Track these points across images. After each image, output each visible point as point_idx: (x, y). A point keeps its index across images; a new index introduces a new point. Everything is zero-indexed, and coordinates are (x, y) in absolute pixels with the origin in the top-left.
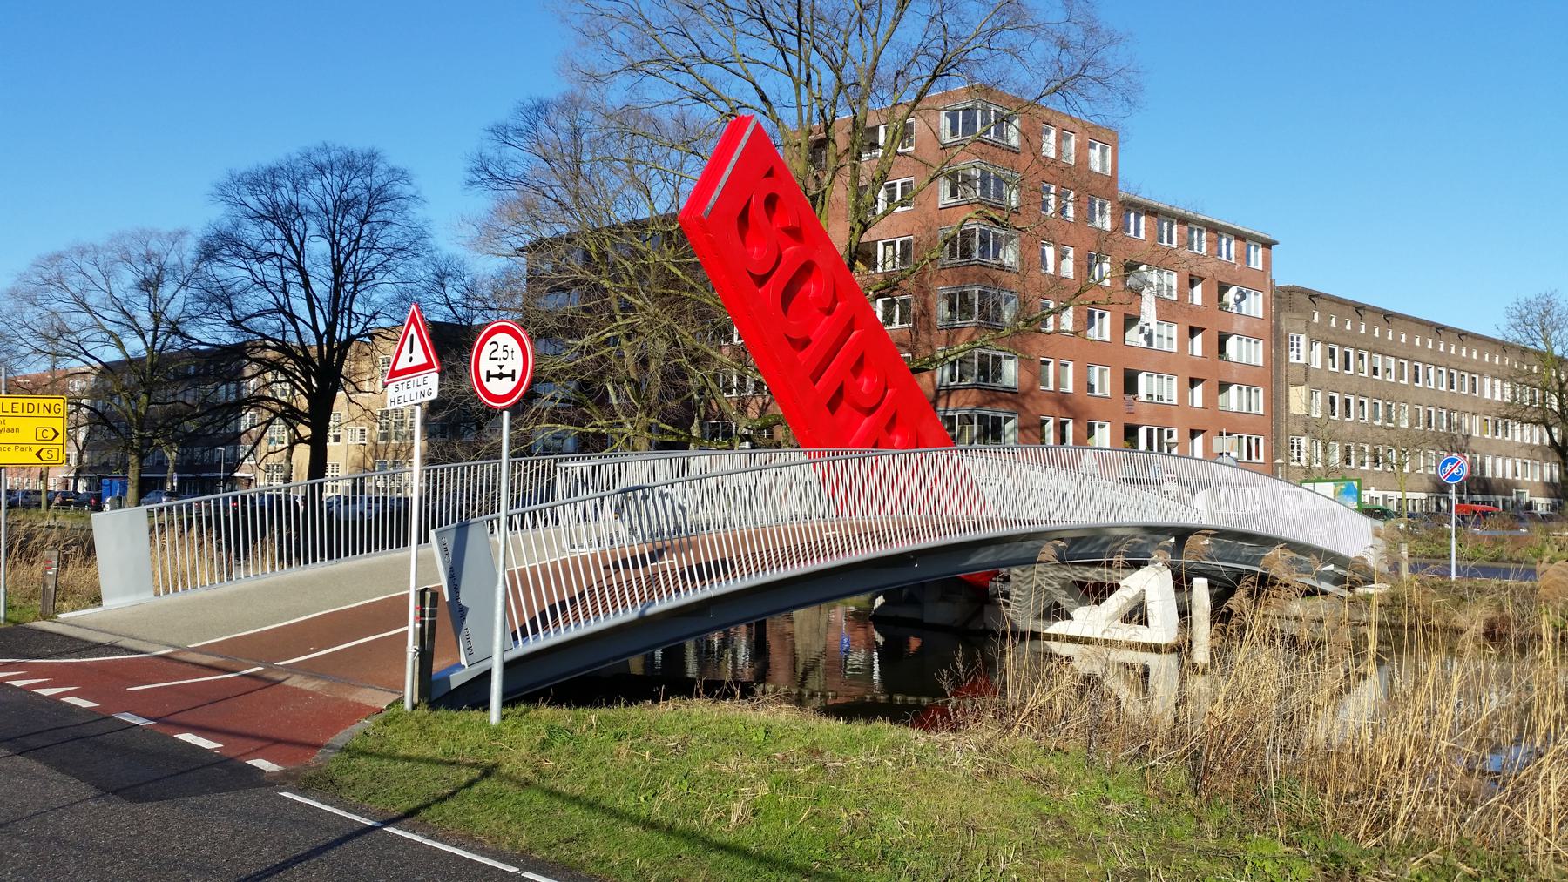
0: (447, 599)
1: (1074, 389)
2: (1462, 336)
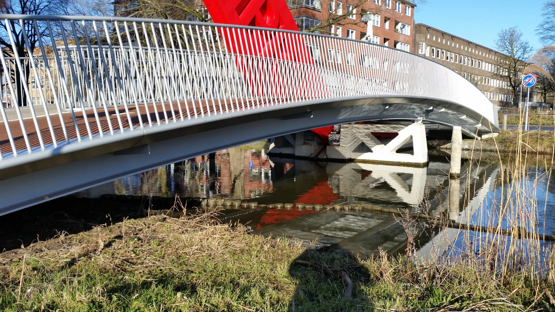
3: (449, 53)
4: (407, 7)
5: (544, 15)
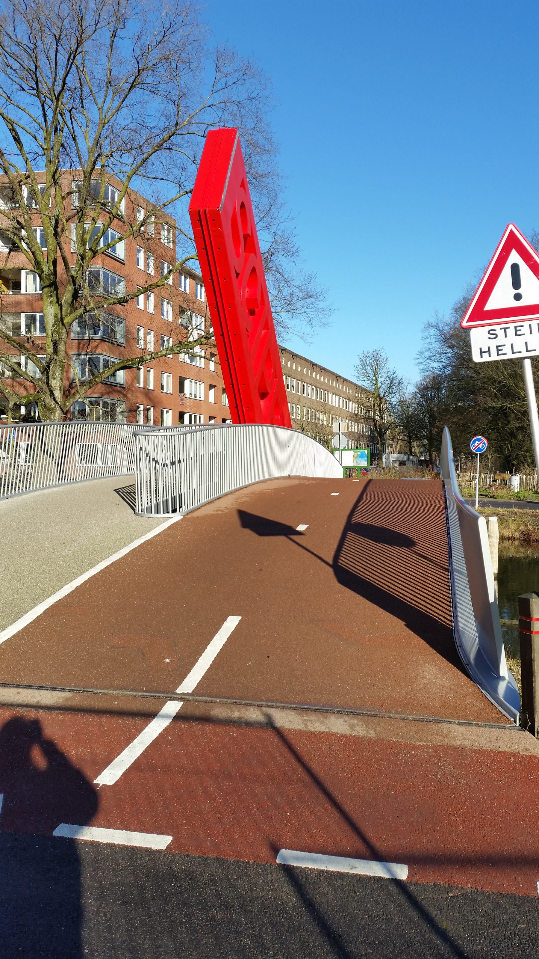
0: (338, 494)
1: (154, 387)
2: (323, 370)
3: (290, 378)
4: (199, 286)
5: (423, 338)
